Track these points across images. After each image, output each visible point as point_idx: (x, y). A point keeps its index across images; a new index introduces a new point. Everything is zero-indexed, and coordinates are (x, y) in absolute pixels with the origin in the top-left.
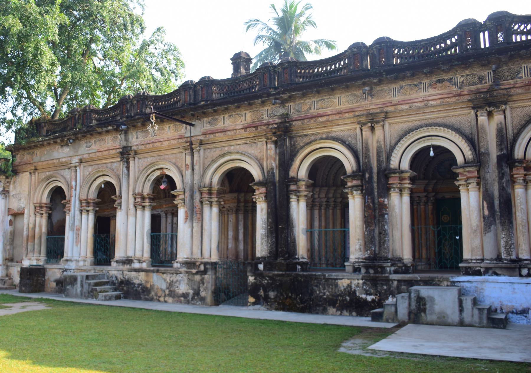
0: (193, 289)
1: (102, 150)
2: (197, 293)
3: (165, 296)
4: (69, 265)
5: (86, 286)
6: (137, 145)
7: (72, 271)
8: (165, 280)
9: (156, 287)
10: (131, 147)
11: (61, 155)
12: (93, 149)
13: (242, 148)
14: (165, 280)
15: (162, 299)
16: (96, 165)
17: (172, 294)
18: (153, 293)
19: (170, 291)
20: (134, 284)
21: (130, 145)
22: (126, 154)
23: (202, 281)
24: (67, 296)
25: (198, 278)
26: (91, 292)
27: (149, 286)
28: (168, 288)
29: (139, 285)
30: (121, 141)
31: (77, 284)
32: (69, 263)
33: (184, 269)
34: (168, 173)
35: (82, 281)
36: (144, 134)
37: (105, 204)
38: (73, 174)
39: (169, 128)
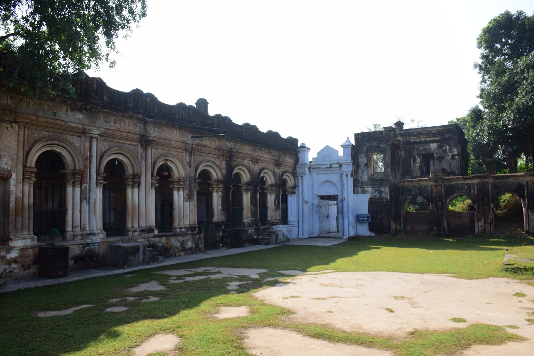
0: (195, 244)
2: (197, 246)
4: (91, 239)
5: (148, 254)
6: (154, 137)
7: (96, 244)
8: (179, 240)
10: (148, 136)
11: (71, 119)
12: (111, 126)
14: (179, 240)
15: (177, 254)
16: (113, 142)
18: (172, 251)
20: (158, 247)
21: (148, 135)
22: (145, 142)
23: (199, 238)
24: (130, 266)
25: (197, 236)
26: (153, 257)
27: (169, 246)
28: (181, 246)
29: (162, 247)
30: (140, 129)
31: (139, 253)
32: (90, 237)
33: (189, 232)
34: (169, 163)
35: (144, 250)
37: (116, 180)
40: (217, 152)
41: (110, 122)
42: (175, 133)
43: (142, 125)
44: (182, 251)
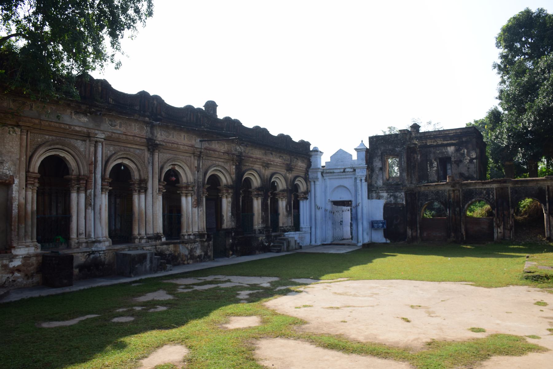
1: (129, 134)
2: (206, 254)
3: (188, 260)
4: (96, 247)
6: (161, 141)
8: (187, 248)
9: (181, 254)
13: (223, 164)
14: (187, 248)
15: (186, 262)
17: (192, 257)
18: (180, 259)
19: (191, 256)
20: (166, 255)
21: (155, 138)
22: (152, 146)
23: (208, 246)
24: (136, 275)
25: (206, 244)
27: (177, 254)
28: (189, 254)
29: (170, 255)
30: (147, 132)
33: (198, 239)
36: (167, 134)
37: (122, 185)
38: (92, 149)
39: (120, 123)
40: (226, 156)
41: (115, 126)
42: (183, 137)
43: (149, 129)
44: (191, 258)
